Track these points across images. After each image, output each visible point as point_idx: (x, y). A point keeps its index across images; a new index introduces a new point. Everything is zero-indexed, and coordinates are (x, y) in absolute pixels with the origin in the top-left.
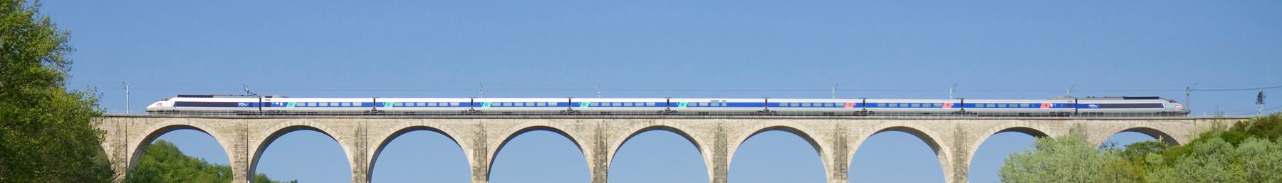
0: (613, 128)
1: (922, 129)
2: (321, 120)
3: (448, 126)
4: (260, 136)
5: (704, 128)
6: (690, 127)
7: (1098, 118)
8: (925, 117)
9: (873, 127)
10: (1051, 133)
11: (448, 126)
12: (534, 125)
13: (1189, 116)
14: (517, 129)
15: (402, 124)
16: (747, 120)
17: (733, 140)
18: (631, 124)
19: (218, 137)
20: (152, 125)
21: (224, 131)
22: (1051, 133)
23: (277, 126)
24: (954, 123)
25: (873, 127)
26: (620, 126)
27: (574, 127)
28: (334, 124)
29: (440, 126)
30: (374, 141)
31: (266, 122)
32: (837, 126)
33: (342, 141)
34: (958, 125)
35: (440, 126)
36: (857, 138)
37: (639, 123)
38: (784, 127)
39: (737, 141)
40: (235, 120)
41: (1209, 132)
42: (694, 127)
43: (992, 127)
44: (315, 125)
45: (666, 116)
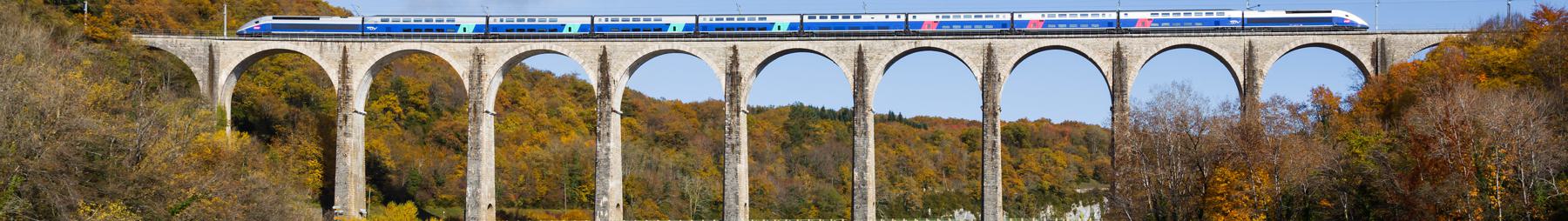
0: (875, 50)
1: (1342, 45)
2: (563, 44)
3: (699, 49)
4: (498, 61)
5: (973, 49)
6: (959, 48)
7: (457, 40)
8: (1213, 34)
9: (1156, 45)
10: (1352, 49)
11: (699, 49)
12: (791, 47)
13: (1368, 31)
14: (773, 52)
15: (650, 48)
16: (1020, 40)
17: (1005, 61)
18: (895, 46)
19: (704, 57)
20: (381, 50)
21: (459, 56)
22: (1352, 49)
23: (253, 49)
24: (1113, 42)
25: (1156, 45)
26: (883, 48)
27: (834, 50)
28: (578, 48)
29: (691, 49)
30: (621, 65)
31: (504, 46)
32: (1118, 44)
33: (586, 65)
34: (1250, 42)
35: (691, 49)
36: (1140, 57)
37: (903, 44)
38: (1332, 45)
39: (1010, 63)
40: (472, 44)
41: (372, 85)
42: (962, 48)
43: (1287, 43)
44: (551, 47)
45: (1001, 36)
